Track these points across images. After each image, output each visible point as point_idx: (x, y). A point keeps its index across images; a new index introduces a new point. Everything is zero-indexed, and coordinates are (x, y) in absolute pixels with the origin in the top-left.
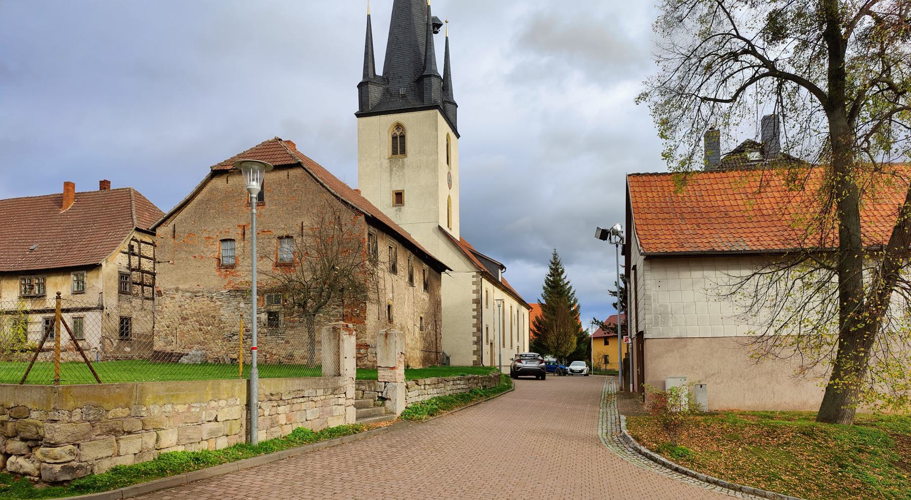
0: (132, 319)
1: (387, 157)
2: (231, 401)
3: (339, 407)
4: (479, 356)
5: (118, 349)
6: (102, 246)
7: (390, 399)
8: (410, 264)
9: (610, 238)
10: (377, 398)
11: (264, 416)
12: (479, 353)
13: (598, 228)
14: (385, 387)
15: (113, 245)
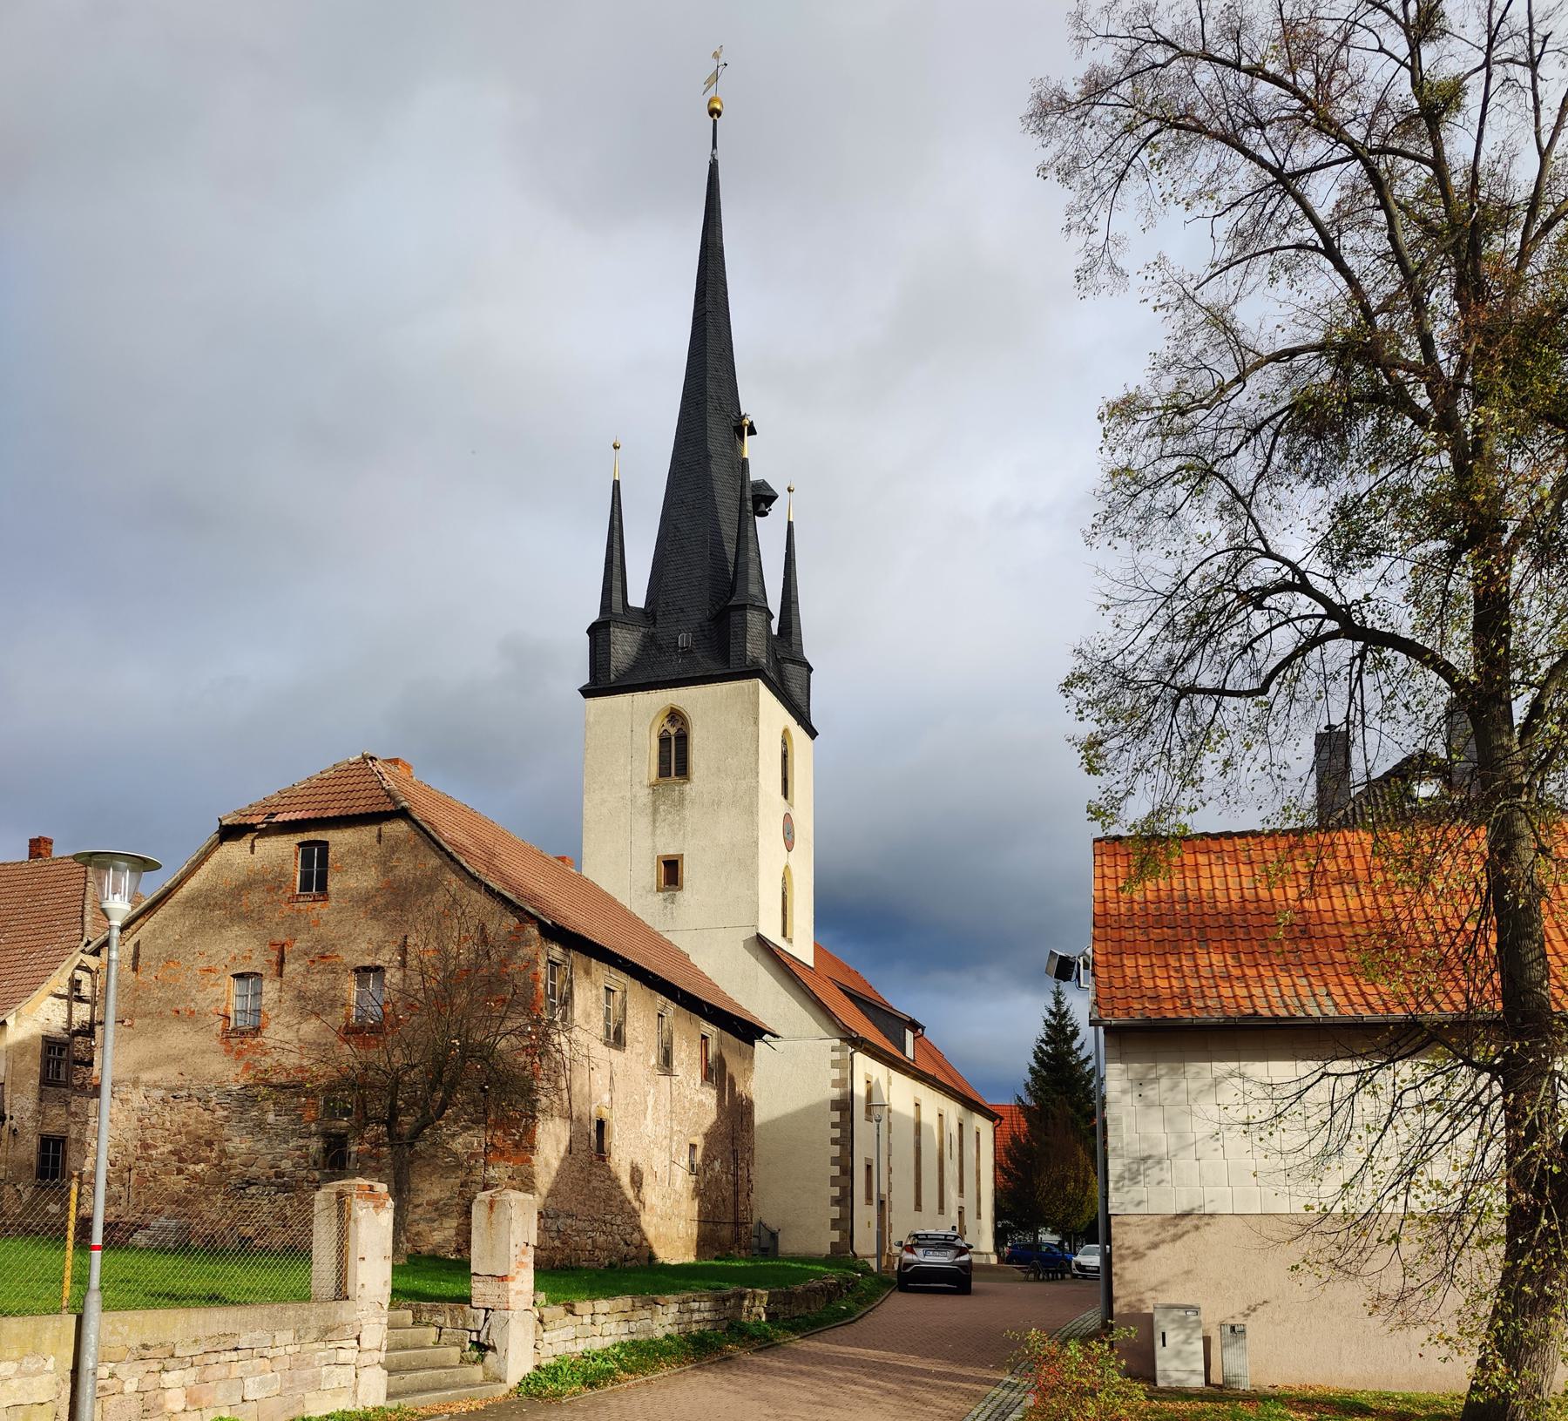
0: (68, 1141)
1: (646, 782)
2: (31, 1364)
3: (338, 1370)
4: (845, 1231)
5: (31, 1206)
6: (13, 983)
7: (494, 1349)
8: (665, 1026)
9: (1078, 977)
10: (468, 1345)
11: (122, 1393)
12: (845, 1224)
13: (1052, 953)
14: (486, 1320)
15: (33, 980)
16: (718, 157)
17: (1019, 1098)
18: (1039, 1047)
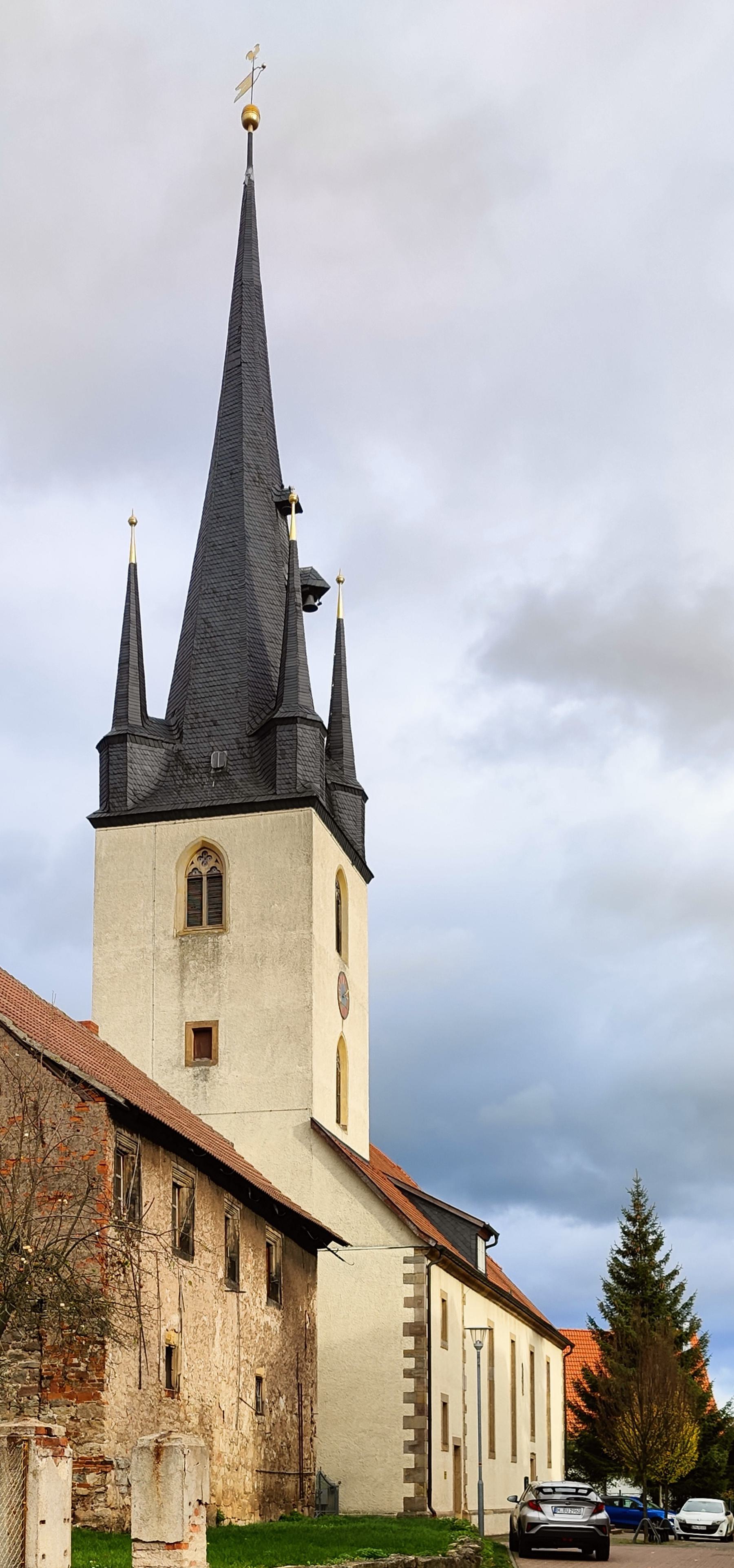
1: (172, 932)
4: (422, 1484)
8: (231, 1231)
16: (255, 178)
17: (592, 1321)
18: (615, 1259)
